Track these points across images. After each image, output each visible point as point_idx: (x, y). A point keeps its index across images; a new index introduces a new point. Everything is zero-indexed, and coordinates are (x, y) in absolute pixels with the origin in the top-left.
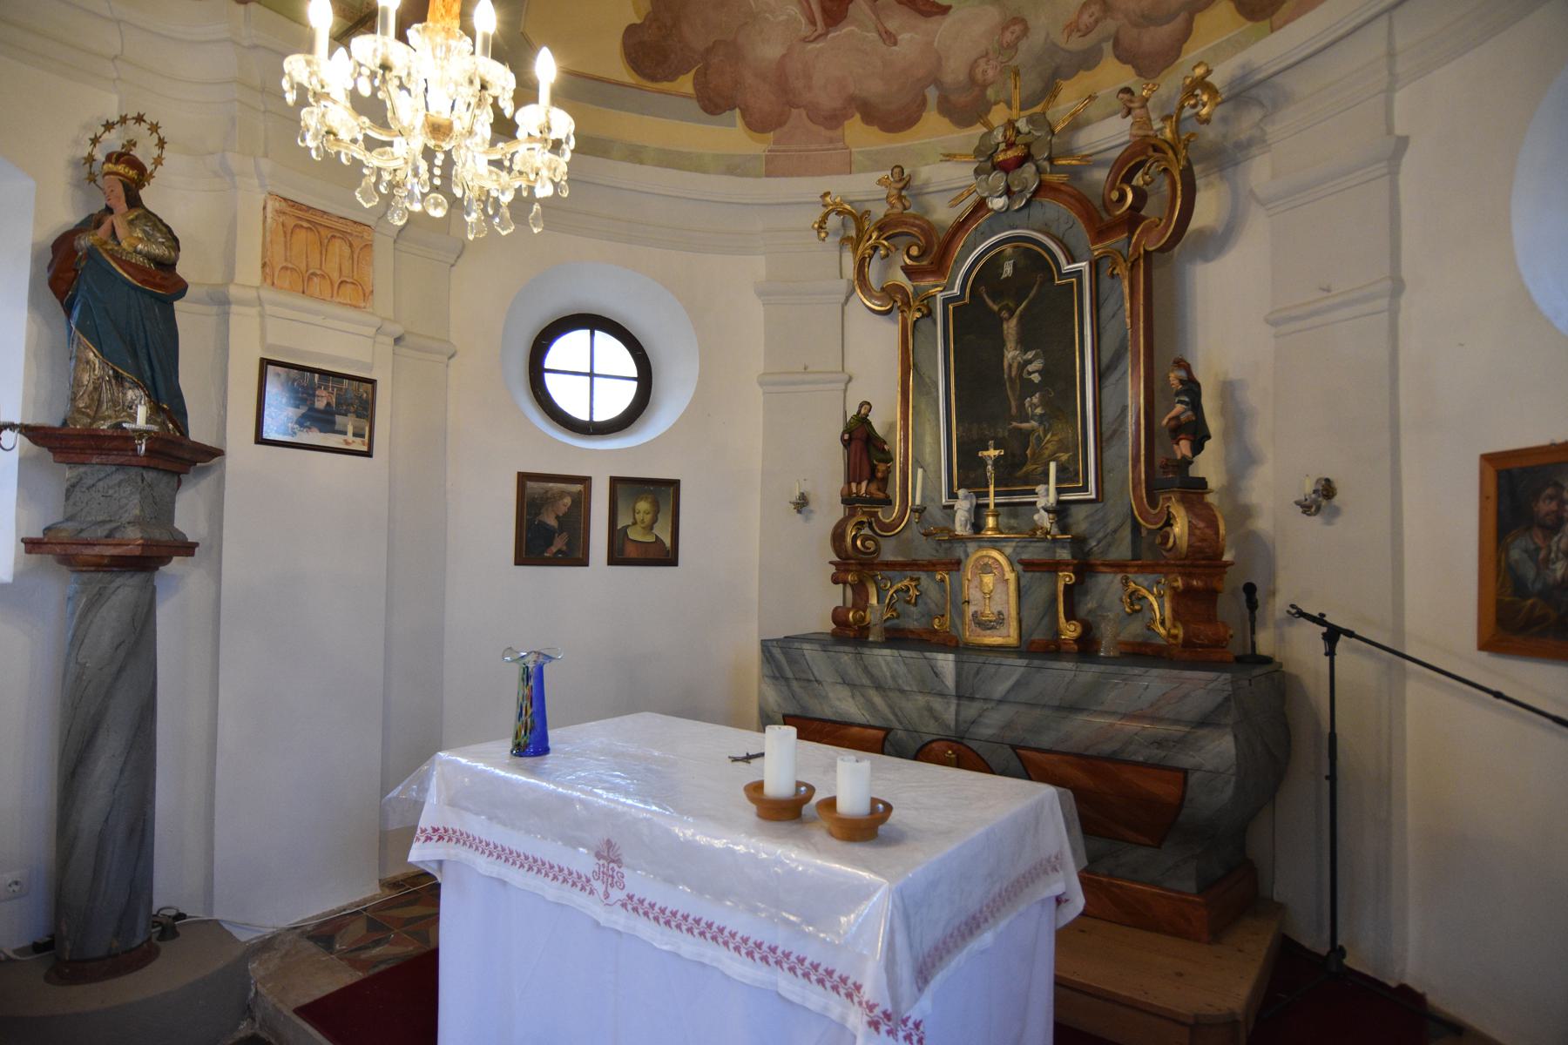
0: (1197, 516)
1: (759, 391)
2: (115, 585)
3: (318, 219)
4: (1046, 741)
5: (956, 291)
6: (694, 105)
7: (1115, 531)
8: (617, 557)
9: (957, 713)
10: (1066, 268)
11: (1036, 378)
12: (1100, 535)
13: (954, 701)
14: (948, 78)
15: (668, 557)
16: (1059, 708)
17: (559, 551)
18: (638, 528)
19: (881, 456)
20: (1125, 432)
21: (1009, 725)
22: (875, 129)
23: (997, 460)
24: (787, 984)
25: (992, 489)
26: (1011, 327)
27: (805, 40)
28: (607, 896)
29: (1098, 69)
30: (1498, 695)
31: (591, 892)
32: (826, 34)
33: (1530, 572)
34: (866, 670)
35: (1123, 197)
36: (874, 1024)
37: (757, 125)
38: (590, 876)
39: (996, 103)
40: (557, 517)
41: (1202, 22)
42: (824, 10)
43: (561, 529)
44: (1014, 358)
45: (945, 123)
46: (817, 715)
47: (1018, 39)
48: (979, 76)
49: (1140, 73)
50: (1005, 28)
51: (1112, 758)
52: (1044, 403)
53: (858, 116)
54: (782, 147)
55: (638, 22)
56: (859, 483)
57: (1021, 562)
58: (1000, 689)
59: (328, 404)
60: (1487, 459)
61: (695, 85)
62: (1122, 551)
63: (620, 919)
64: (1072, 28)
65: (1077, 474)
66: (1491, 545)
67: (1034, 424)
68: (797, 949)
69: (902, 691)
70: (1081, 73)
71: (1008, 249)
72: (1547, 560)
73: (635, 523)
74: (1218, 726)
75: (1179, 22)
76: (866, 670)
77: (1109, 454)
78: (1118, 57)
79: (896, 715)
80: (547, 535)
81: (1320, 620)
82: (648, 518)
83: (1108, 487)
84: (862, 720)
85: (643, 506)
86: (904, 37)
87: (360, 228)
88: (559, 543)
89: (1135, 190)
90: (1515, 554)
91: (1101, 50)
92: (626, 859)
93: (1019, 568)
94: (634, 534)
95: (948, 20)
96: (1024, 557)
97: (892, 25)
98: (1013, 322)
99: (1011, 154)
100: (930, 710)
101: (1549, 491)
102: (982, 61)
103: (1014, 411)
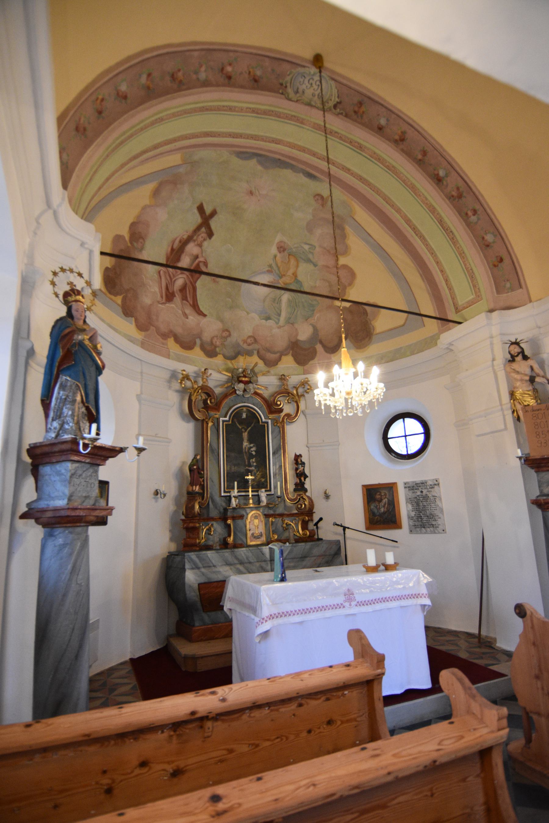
5: (227, 419)
6: (120, 310)
11: (254, 453)
13: (269, 563)
14: (204, 339)
16: (301, 558)
22: (178, 345)
23: (253, 480)
24: (403, 603)
25: (250, 490)
26: (245, 435)
27: (158, 302)
28: (350, 605)
29: (252, 357)
30: (381, 537)
31: (344, 607)
33: (376, 511)
34: (236, 558)
38: (342, 602)
39: (220, 354)
41: (284, 358)
42: (167, 295)
44: (247, 445)
45: (201, 353)
46: (216, 580)
47: (227, 337)
48: (214, 342)
50: (223, 331)
52: (256, 462)
53: (172, 339)
54: (147, 340)
56: (196, 486)
60: (364, 486)
61: (122, 302)
63: (355, 610)
64: (245, 341)
66: (366, 506)
67: (253, 468)
69: (250, 563)
71: (245, 409)
72: (379, 508)
75: (278, 355)
76: (236, 558)
86: (190, 317)
90: (372, 507)
91: (253, 352)
96: (265, 513)
98: (246, 433)
99: (247, 379)
101: (378, 493)
102: (215, 339)
103: (247, 463)
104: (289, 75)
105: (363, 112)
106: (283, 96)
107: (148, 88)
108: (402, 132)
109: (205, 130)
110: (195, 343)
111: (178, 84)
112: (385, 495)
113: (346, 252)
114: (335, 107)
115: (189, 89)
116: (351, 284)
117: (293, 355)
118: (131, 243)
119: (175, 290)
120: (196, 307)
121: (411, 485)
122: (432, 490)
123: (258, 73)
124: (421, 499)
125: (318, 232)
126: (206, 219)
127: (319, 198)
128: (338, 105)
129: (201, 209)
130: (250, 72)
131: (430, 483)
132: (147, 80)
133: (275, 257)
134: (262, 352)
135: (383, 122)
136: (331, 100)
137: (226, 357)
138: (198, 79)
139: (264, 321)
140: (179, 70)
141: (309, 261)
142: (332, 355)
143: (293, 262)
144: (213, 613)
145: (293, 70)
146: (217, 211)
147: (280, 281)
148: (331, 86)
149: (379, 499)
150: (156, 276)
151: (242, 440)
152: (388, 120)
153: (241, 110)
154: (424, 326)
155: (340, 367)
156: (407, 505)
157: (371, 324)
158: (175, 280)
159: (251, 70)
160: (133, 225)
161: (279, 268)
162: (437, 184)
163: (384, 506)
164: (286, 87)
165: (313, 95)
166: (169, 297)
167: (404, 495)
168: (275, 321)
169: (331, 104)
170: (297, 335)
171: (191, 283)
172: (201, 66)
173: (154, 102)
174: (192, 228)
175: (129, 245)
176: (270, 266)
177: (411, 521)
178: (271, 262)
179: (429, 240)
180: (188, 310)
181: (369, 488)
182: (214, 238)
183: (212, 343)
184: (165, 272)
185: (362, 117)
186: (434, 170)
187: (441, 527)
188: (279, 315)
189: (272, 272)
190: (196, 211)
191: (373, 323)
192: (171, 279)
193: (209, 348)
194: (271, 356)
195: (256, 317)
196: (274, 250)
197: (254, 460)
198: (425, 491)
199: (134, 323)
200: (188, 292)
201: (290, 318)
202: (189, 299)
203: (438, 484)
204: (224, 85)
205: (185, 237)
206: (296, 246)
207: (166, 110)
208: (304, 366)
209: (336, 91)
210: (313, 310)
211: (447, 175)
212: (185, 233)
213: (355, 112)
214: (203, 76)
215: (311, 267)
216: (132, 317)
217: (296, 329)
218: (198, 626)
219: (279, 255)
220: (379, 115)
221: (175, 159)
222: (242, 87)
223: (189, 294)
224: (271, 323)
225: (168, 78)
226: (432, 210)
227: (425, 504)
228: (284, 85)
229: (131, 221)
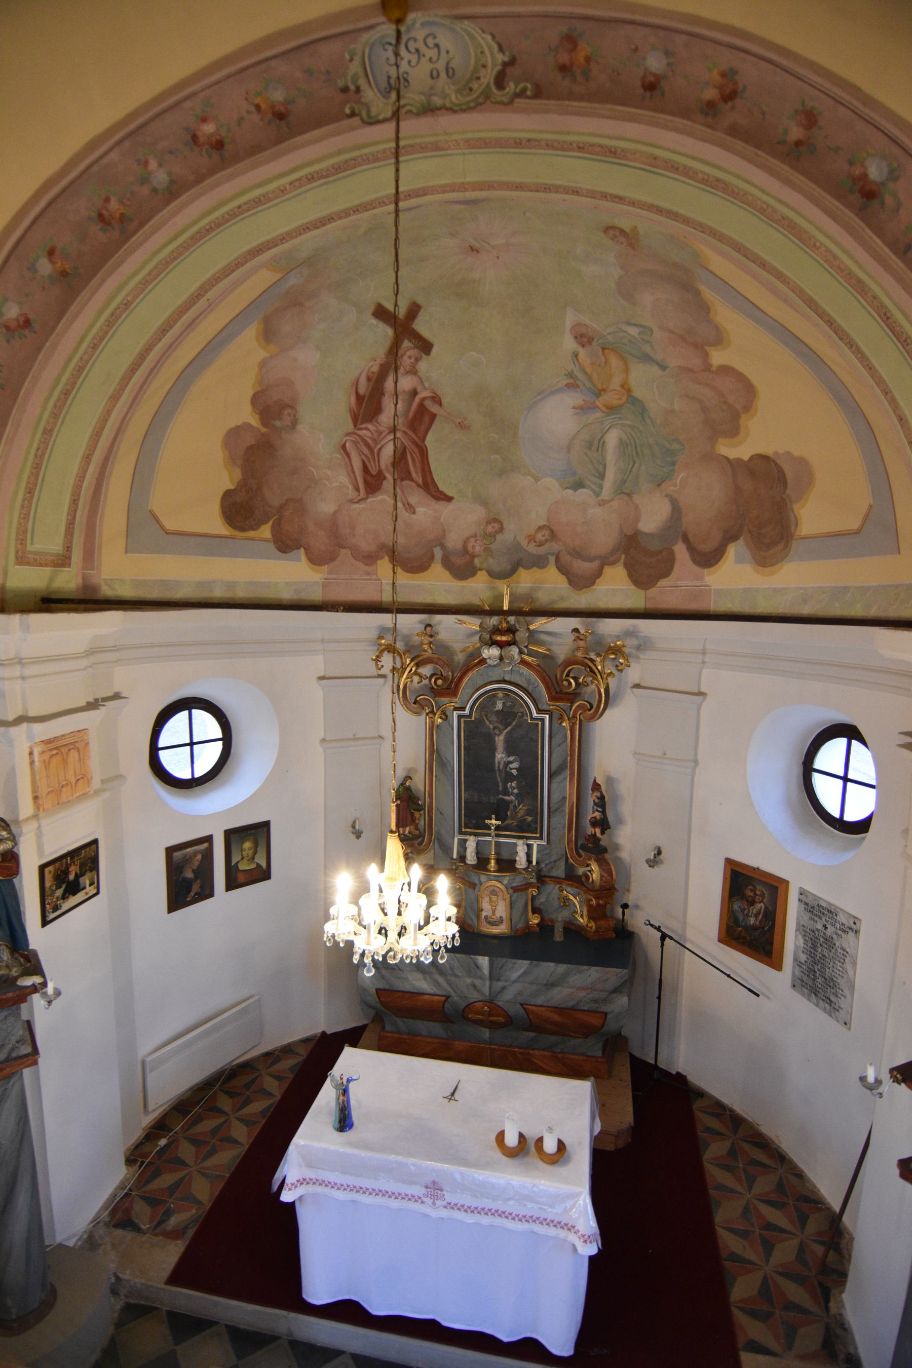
0: (604, 870)
1: (320, 750)
2: (11, 1083)
3: (60, 743)
4: (539, 1001)
5: (467, 712)
6: (271, 547)
7: (555, 861)
8: (232, 884)
9: (490, 988)
10: (535, 715)
11: (514, 772)
12: (547, 862)
15: (263, 874)
17: (196, 894)
18: (245, 861)
19: (416, 807)
20: (563, 811)
21: (520, 993)
26: (500, 740)
27: (352, 501)
28: (434, 1204)
30: (729, 976)
31: (423, 1202)
32: (366, 498)
35: (570, 683)
36: (585, 1241)
37: (316, 560)
39: (480, 570)
40: (193, 871)
41: (608, 571)
42: (366, 482)
43: (196, 878)
44: (502, 758)
47: (497, 532)
48: (470, 548)
49: (571, 582)
50: (488, 523)
51: (572, 1009)
52: (518, 787)
53: (387, 558)
54: (334, 576)
55: (232, 487)
57: (512, 888)
58: (515, 976)
59: (76, 874)
61: (272, 531)
62: (560, 872)
63: (445, 1213)
64: (531, 539)
65: (536, 829)
67: (512, 798)
68: (543, 1216)
70: (535, 569)
71: (500, 694)
73: (243, 858)
74: (621, 992)
75: (595, 565)
77: (554, 820)
78: (558, 568)
79: (452, 988)
80: (188, 884)
81: (658, 929)
82: (251, 853)
83: (552, 837)
84: (432, 992)
85: (247, 845)
86: (420, 510)
87: (82, 733)
88: (196, 888)
89: (573, 678)
90: (736, 907)
92: (445, 1188)
93: (511, 891)
94: (242, 867)
95: (451, 506)
96: (514, 885)
97: (413, 500)
98: (502, 738)
100: (474, 986)
102: (473, 540)
103: (501, 788)
104: (351, 60)
105: (588, 59)
106: (356, 121)
107: (64, 274)
108: (723, 75)
109: (248, 247)
110: (432, 558)
111: (119, 226)
112: (763, 895)
113: (719, 339)
114: (500, 81)
115: (142, 225)
116: (748, 407)
117: (626, 565)
118: (265, 423)
119: (383, 467)
120: (431, 487)
121: (809, 900)
122: (843, 935)
123: (278, 96)
124: (822, 939)
125: (647, 299)
126: (403, 326)
127: (618, 233)
128: (509, 71)
129: (381, 313)
130: (258, 107)
131: (842, 918)
132: (52, 262)
133: (576, 355)
134: (566, 558)
135: (655, 63)
136: (484, 66)
137: (493, 575)
138: (155, 190)
139: (570, 492)
140: (107, 200)
141: (647, 358)
142: (706, 571)
143: (614, 361)
144: (411, 1021)
145: (352, 46)
146: (419, 303)
147: (598, 404)
148: (471, 36)
149: (750, 899)
150: (339, 456)
151: (493, 750)
152: (667, 53)
153: (283, 191)
154: (899, 553)
155: (382, 869)
156: (796, 936)
157: (792, 510)
158: (380, 449)
159: (258, 100)
160: (256, 399)
161: (589, 377)
162: (861, 212)
163: (756, 916)
164: (358, 90)
165: (434, 76)
166: (372, 483)
167: (795, 916)
168: (593, 491)
169: (488, 77)
170: (638, 520)
171: (415, 443)
172: (146, 163)
173: (85, 293)
174: (380, 352)
175: (264, 430)
176: (570, 375)
177: (798, 968)
178: (570, 367)
179: (871, 358)
180: (416, 497)
181: (738, 869)
182: (434, 351)
183: (465, 550)
184: (355, 443)
185: (586, 75)
186: (851, 163)
187: (842, 1014)
188: (602, 476)
189: (578, 386)
190: (374, 321)
191: (796, 507)
192: (371, 450)
193: (459, 561)
194: (582, 567)
195: (550, 482)
196: (569, 344)
197: (514, 784)
198: (830, 930)
199: (303, 557)
200: (410, 462)
201: (624, 482)
202: (414, 475)
203: (857, 932)
204: (213, 171)
205: (375, 369)
206: (611, 330)
207: (119, 289)
208: (646, 589)
209: (489, 37)
210: (673, 464)
211: (893, 175)
212: (372, 363)
213: (564, 69)
214: (161, 177)
215: (656, 369)
216: (298, 548)
217: (637, 507)
218: (389, 1032)
219: (582, 353)
220: (636, 49)
221: (264, 279)
222: (256, 149)
223: (411, 467)
224: (583, 494)
225: (95, 228)
226: (860, 287)
227: (826, 953)
228: (352, 87)
229: (250, 393)
